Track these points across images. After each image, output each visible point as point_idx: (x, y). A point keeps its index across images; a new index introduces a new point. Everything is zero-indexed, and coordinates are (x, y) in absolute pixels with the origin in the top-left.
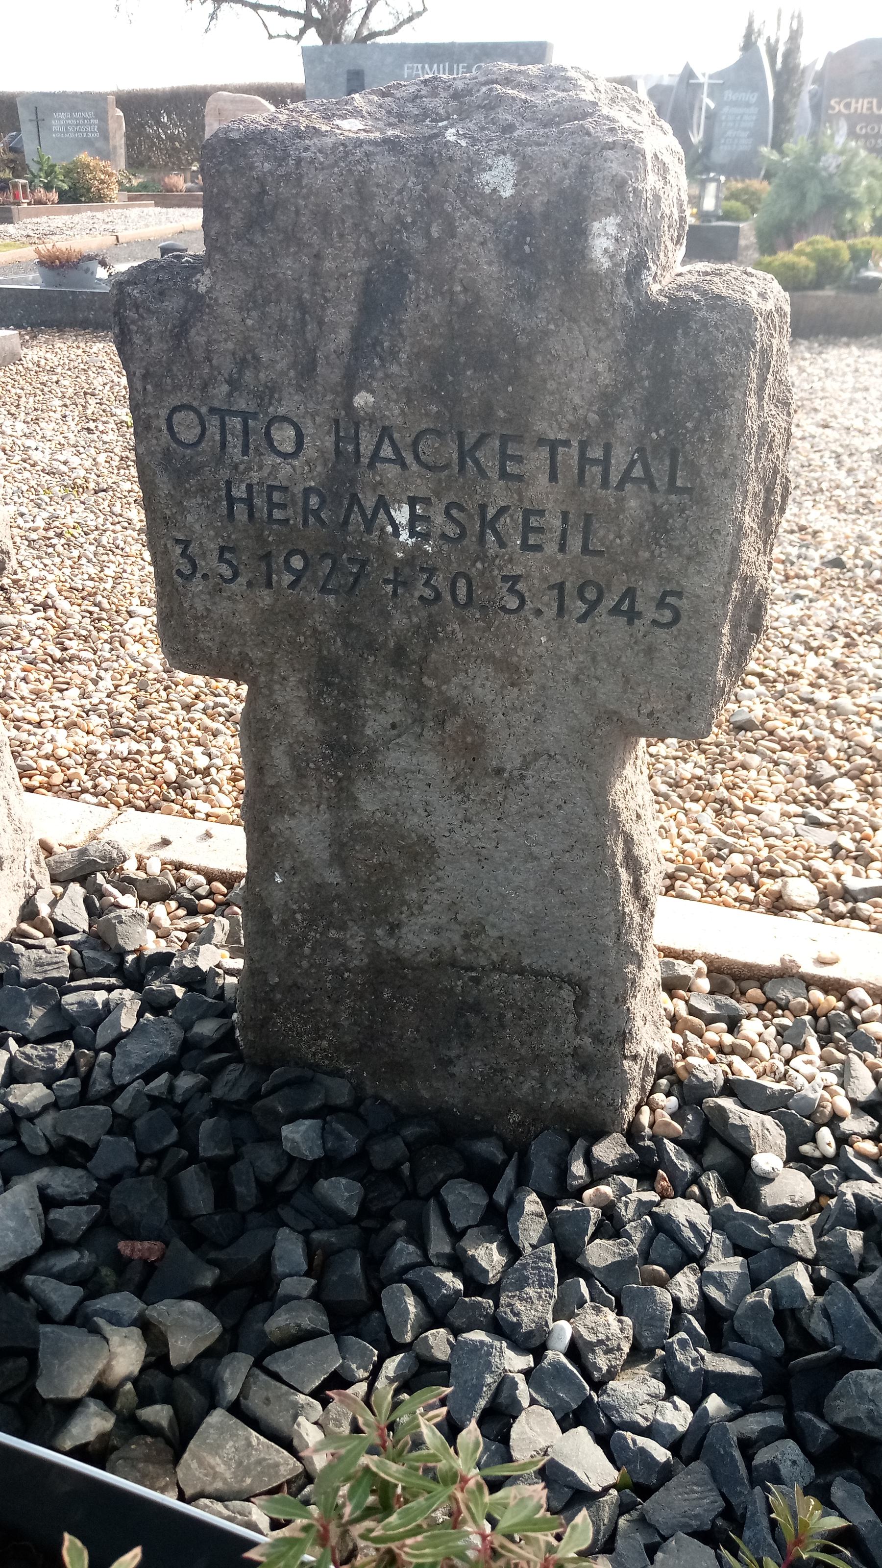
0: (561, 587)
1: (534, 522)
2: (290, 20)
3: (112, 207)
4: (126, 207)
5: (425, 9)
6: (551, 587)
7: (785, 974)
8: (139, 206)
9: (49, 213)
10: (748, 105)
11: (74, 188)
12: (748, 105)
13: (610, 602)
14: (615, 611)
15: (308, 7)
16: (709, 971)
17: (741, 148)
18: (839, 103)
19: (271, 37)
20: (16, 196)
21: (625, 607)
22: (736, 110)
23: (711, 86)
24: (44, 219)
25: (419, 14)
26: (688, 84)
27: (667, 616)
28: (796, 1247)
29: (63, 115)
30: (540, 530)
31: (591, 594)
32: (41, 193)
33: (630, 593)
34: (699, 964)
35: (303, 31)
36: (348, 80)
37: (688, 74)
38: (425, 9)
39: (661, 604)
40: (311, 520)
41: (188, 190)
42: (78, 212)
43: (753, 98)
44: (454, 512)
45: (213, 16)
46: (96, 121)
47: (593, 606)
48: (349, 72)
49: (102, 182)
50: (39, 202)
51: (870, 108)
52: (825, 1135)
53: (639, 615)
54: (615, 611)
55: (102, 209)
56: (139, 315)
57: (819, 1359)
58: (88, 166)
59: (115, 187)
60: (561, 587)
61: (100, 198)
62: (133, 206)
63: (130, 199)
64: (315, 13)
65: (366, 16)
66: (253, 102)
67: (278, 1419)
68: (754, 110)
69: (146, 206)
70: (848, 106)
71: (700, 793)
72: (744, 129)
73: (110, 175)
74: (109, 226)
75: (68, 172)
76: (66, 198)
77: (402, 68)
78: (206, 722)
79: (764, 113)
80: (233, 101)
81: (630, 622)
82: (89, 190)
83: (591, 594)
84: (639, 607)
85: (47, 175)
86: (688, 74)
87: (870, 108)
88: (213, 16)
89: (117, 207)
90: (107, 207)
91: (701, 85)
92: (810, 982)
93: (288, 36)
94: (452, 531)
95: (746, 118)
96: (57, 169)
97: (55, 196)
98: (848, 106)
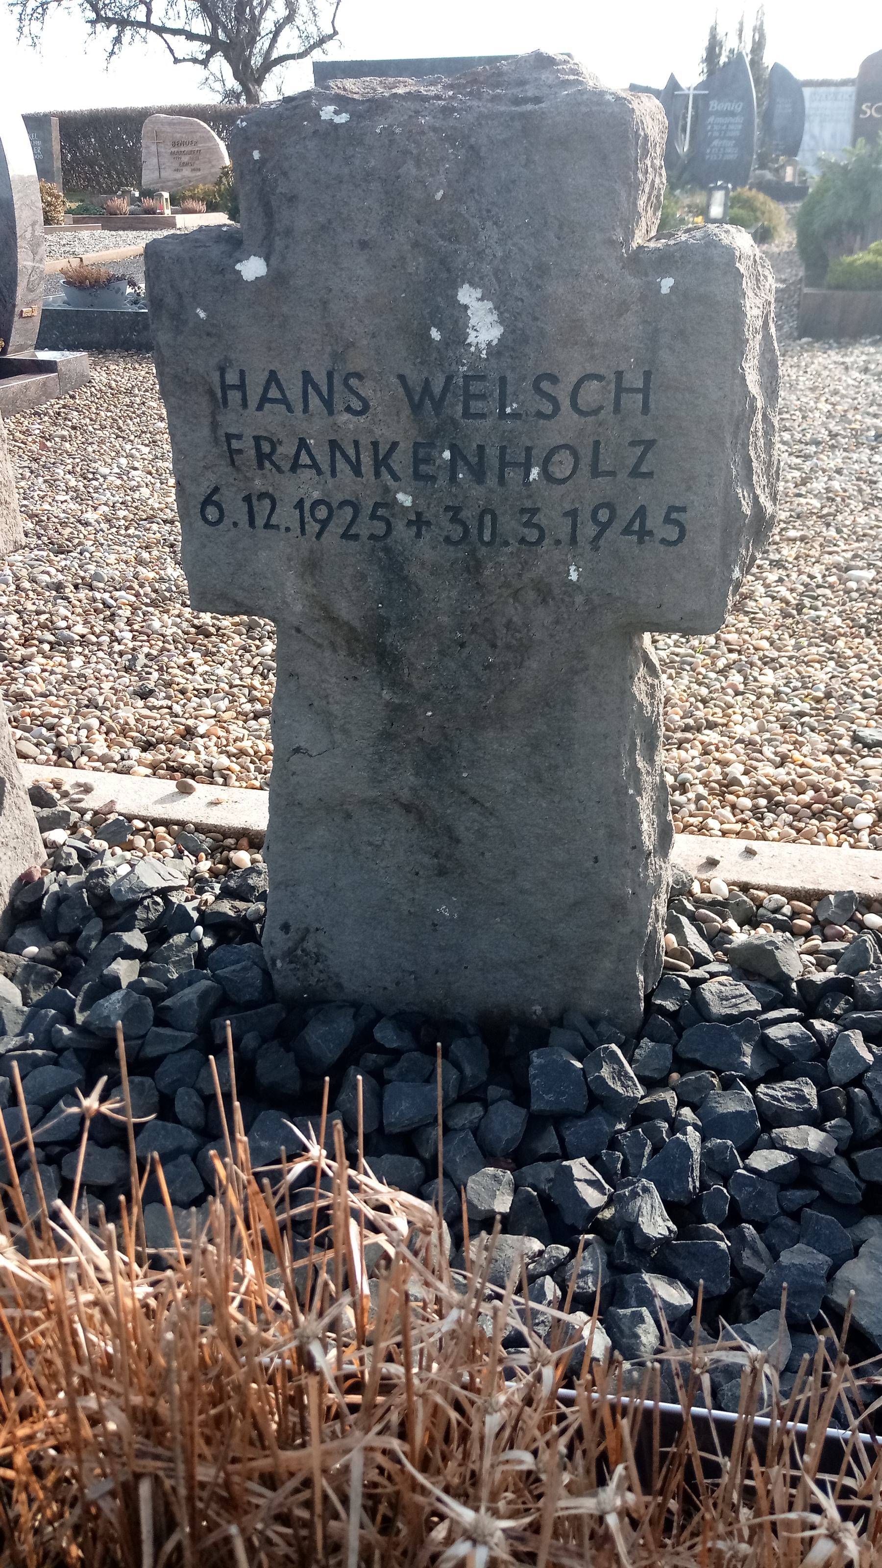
2: (197, 43)
4: (75, 230)
5: (335, 33)
6: (566, 514)
8: (87, 229)
10: (733, 114)
12: (733, 114)
15: (214, 30)
17: (727, 157)
19: (176, 61)
21: (636, 526)
22: (720, 120)
23: (695, 96)
25: (330, 37)
27: (673, 533)
33: (641, 512)
35: (210, 54)
38: (335, 33)
41: (132, 213)
43: (738, 107)
45: (118, 40)
47: (604, 527)
53: (650, 533)
54: (627, 531)
62: (81, 229)
63: (76, 221)
64: (222, 36)
65: (274, 41)
66: (192, 124)
68: (739, 120)
69: (94, 229)
72: (730, 138)
78: (231, 680)
79: (749, 123)
80: (171, 123)
81: (641, 541)
83: (603, 515)
84: (649, 525)
88: (118, 40)
90: (55, 230)
93: (195, 60)
95: (731, 127)
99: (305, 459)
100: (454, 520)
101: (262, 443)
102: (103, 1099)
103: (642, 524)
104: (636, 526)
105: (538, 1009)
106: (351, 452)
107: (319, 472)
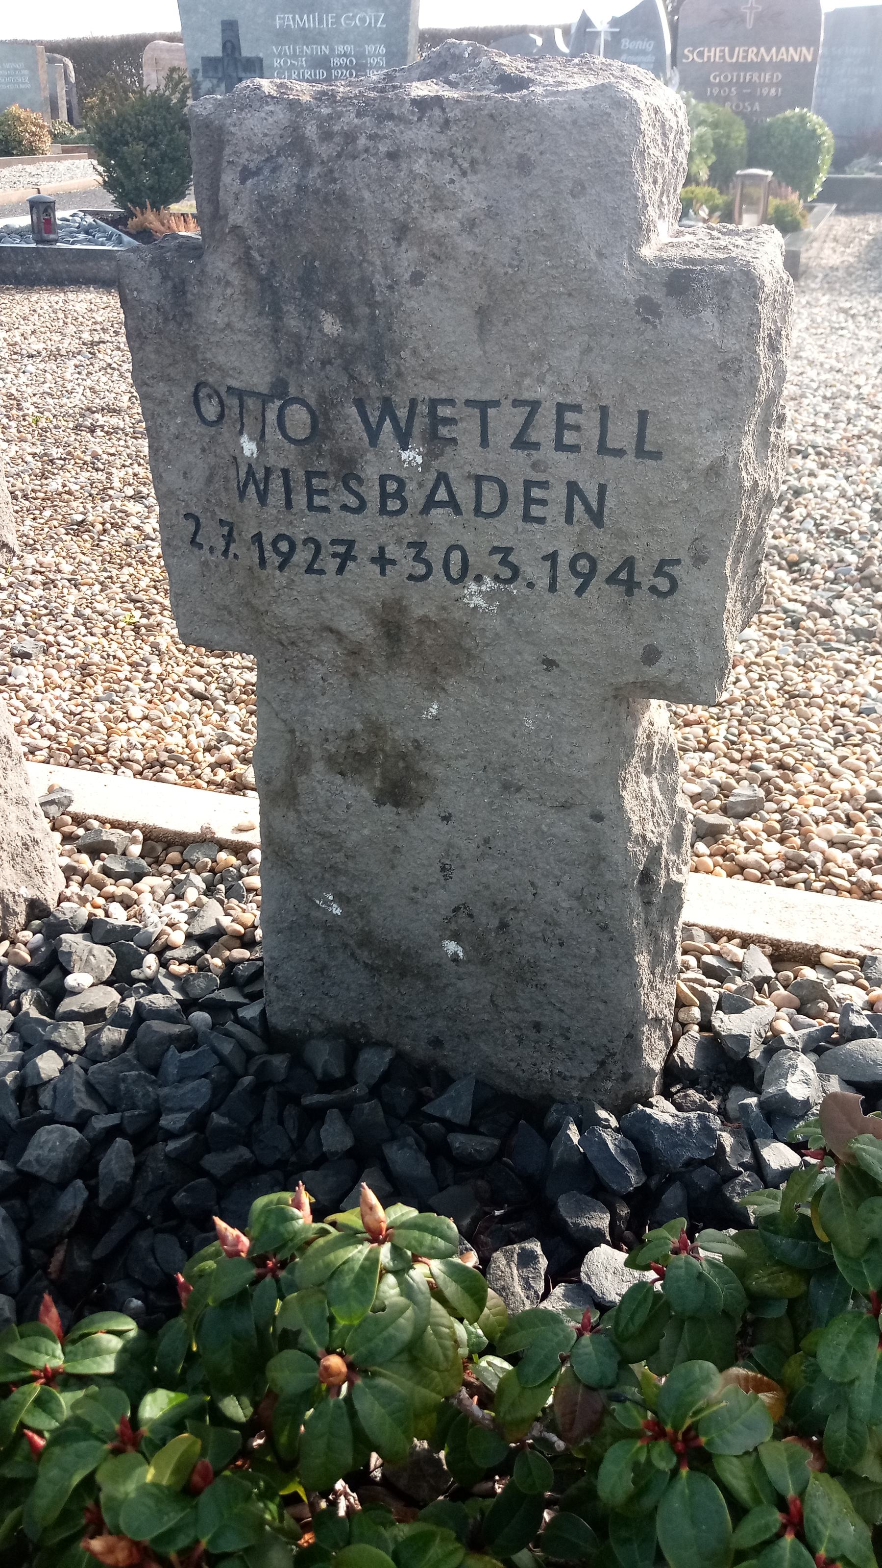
0: (552, 557)
1: (536, 493)
3: (44, 160)
4: (59, 159)
6: (545, 558)
7: (206, 840)
8: (72, 158)
14: (612, 579)
16: (145, 840)
18: (692, 52)
21: (623, 576)
27: (663, 584)
28: (59, 1040)
30: (543, 502)
34: (137, 833)
36: (223, 31)
37: (585, 21)
39: (659, 572)
43: (649, 46)
46: (26, 72)
47: (587, 579)
48: (224, 23)
49: (34, 134)
51: (723, 57)
52: (151, 960)
54: (612, 579)
55: (33, 162)
58: (19, 118)
59: (48, 139)
60: (552, 557)
61: (30, 151)
62: (65, 159)
63: (64, 151)
67: (345, 1424)
69: (80, 158)
70: (701, 54)
71: (244, 697)
73: (42, 127)
74: (34, 180)
78: (214, 702)
80: (169, 50)
82: (20, 143)
86: (585, 21)
87: (723, 57)
89: (49, 159)
90: (39, 160)
91: (597, 34)
92: (222, 845)
98: (701, 54)
99: (442, 495)
100: (417, 558)
101: (486, 486)
102: (390, 1512)
103: (631, 574)
104: (623, 576)
105: (765, 1397)
106: (578, 506)
107: (457, 510)
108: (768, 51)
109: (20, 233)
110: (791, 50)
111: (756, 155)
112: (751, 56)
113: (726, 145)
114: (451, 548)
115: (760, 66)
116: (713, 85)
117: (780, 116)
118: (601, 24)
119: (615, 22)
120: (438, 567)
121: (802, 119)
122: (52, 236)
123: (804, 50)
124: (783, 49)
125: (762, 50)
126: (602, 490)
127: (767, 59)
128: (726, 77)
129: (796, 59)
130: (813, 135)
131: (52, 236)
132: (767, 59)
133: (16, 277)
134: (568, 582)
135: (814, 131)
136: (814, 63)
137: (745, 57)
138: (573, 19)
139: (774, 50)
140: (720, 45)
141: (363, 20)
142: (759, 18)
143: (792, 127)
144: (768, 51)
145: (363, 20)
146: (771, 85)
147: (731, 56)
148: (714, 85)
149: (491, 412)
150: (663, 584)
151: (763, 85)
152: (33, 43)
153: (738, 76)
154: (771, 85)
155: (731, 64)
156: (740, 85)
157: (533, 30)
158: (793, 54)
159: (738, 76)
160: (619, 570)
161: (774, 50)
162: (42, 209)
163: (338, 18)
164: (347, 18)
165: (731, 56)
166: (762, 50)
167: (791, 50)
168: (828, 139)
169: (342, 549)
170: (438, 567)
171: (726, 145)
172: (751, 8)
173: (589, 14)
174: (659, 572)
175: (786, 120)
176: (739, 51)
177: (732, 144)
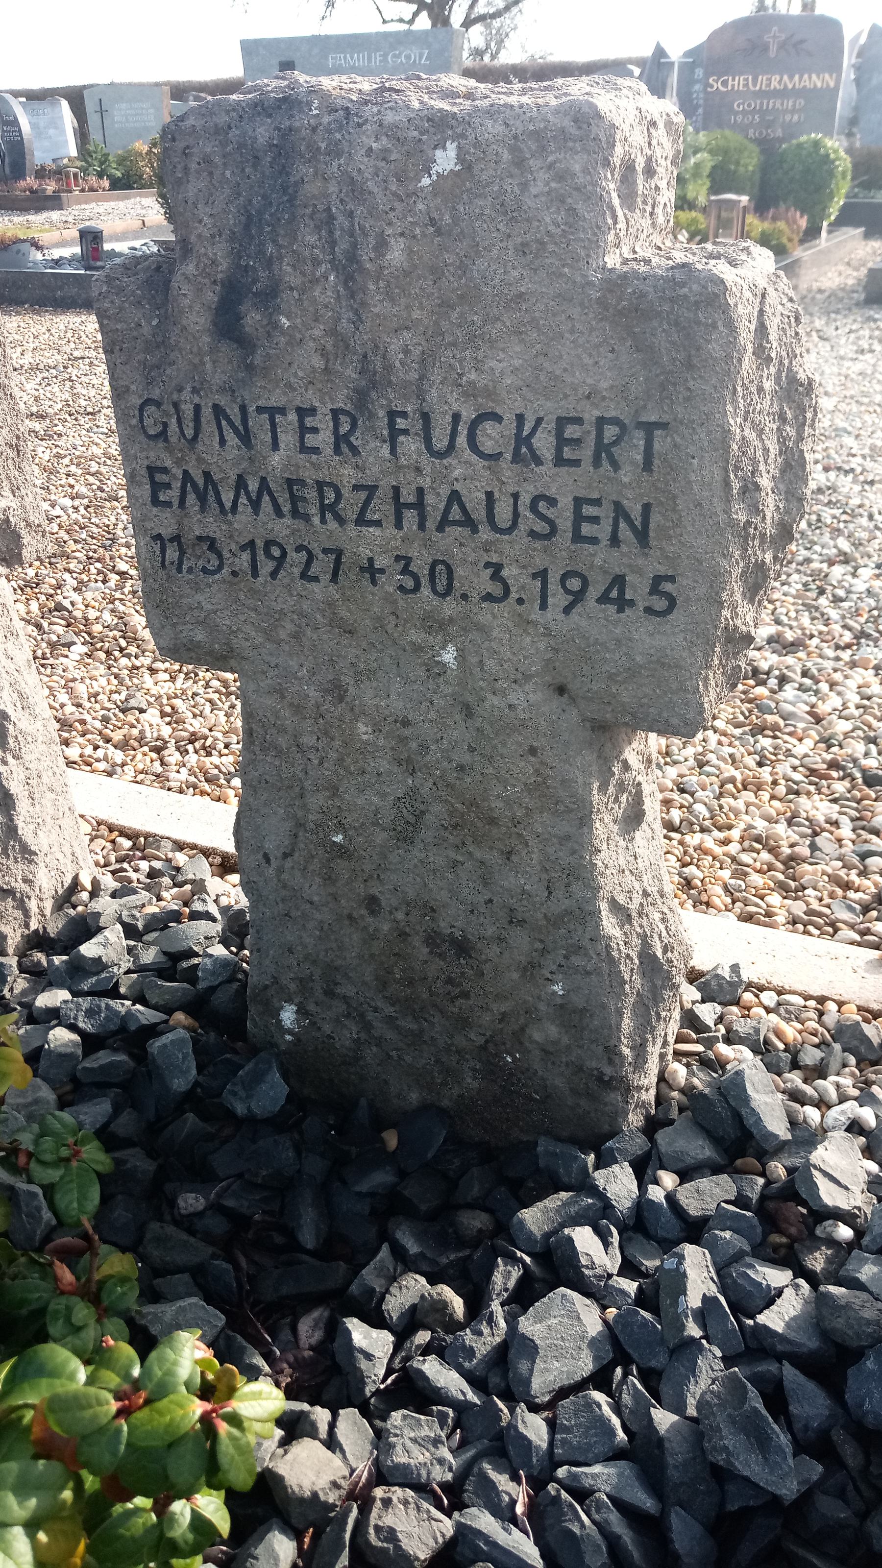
9: (97, 200)
11: (127, 175)
13: (594, 592)
14: (604, 599)
20: (68, 185)
21: (614, 594)
24: (94, 205)
26: (659, 64)
27: (660, 604)
29: (123, 106)
30: (595, 520)
31: (574, 584)
32: (93, 180)
33: (619, 581)
37: (660, 52)
40: (329, 516)
42: (128, 198)
44: (542, 506)
46: (152, 111)
47: (578, 597)
50: (92, 190)
51: (746, 85)
54: (604, 599)
56: (125, 299)
57: (345, 1531)
75: (121, 161)
76: (117, 185)
77: (327, 58)
82: (141, 177)
85: (101, 164)
86: (660, 52)
87: (746, 85)
91: (673, 64)
94: (541, 527)
96: (111, 158)
97: (106, 183)
98: (725, 83)
99: (456, 513)
103: (622, 592)
104: (614, 594)
108: (791, 78)
109: (71, 261)
110: (814, 77)
111: (772, 183)
112: (774, 84)
113: (735, 172)
114: (435, 563)
115: (783, 94)
116: (737, 113)
117: (794, 142)
118: (675, 54)
119: (687, 54)
120: (424, 581)
121: (817, 144)
122: (99, 264)
123: (827, 76)
124: (806, 76)
125: (785, 77)
126: (647, 508)
127: (790, 86)
128: (749, 105)
129: (819, 85)
130: (826, 160)
131: (99, 264)
132: (790, 86)
133: (55, 300)
134: (558, 599)
135: (828, 155)
136: (837, 89)
137: (769, 85)
138: (647, 52)
139: (797, 77)
140: (741, 74)
141: (408, 57)
142: (782, 46)
143: (804, 152)
144: (791, 78)
145: (408, 57)
146: (793, 111)
147: (755, 85)
148: (737, 113)
149: (658, 433)
150: (660, 604)
151: (786, 111)
152: (157, 85)
153: (762, 104)
154: (793, 111)
155: (754, 93)
156: (763, 113)
157: (631, 61)
158: (816, 81)
159: (762, 104)
160: (608, 590)
161: (797, 77)
162: (90, 238)
163: (385, 56)
164: (395, 56)
165: (755, 85)
166: (785, 77)
167: (814, 77)
168: (844, 163)
169: (172, 554)
170: (424, 581)
171: (735, 172)
172: (774, 37)
173: (663, 45)
174: (655, 590)
175: (800, 146)
176: (762, 79)
177: (742, 169)
